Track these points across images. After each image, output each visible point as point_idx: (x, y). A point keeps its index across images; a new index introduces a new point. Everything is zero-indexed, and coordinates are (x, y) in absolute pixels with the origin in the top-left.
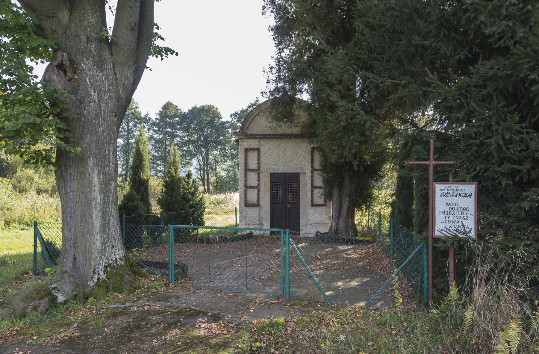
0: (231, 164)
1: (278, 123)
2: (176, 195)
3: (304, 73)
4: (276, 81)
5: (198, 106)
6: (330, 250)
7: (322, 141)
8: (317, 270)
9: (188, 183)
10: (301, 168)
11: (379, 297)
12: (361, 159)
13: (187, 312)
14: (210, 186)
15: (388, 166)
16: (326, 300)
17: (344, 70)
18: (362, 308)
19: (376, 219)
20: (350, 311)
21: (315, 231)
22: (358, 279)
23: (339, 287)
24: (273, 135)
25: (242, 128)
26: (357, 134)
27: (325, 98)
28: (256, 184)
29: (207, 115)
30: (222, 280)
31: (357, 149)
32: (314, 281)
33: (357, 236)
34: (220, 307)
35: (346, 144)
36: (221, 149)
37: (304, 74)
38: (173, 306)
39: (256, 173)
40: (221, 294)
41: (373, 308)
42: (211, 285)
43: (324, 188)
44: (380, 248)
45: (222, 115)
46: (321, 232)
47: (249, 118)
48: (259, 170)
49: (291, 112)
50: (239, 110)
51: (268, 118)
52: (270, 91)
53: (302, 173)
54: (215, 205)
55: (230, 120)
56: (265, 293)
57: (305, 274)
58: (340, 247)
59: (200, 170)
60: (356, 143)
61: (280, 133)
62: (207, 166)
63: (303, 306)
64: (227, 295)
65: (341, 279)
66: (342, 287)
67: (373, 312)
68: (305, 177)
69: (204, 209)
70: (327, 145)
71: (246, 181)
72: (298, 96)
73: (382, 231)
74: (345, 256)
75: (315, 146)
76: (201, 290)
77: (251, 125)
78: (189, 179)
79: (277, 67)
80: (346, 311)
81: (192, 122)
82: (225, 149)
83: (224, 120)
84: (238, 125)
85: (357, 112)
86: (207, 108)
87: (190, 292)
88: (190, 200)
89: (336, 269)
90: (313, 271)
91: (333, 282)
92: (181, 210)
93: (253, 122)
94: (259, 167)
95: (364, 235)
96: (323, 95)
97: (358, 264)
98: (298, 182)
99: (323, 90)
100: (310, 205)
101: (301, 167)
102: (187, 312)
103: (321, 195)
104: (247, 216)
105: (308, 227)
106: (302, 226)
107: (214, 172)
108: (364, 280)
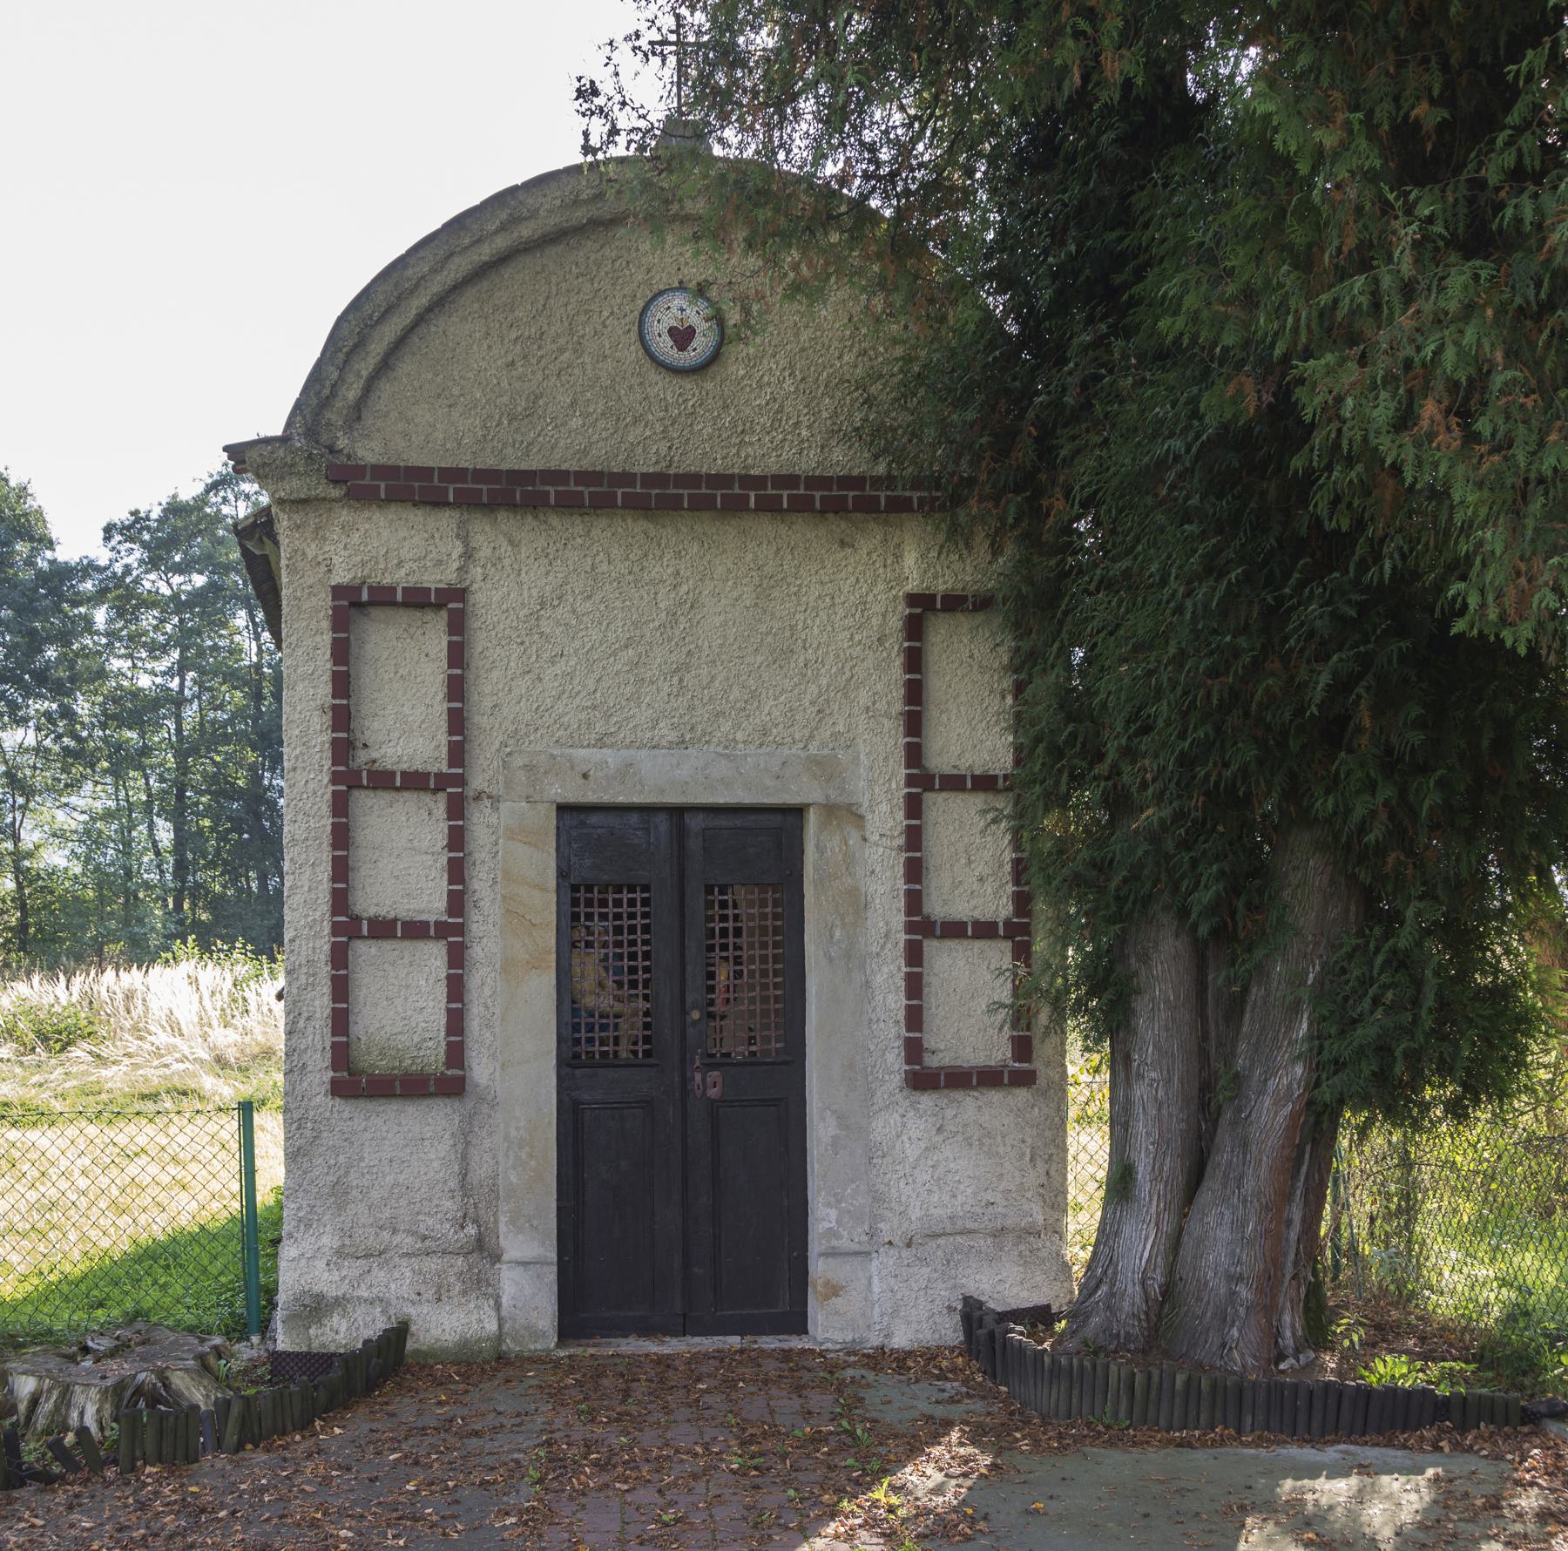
10: (824, 768)
21: (946, 1294)
28: (431, 902)
36: (47, 715)
39: (439, 805)
48: (461, 781)
55: (103, 556)
71: (341, 870)
77: (386, 389)
82: (67, 713)
83: (67, 552)
84: (148, 585)
93: (406, 367)
94: (457, 754)
100: (897, 1079)
104: (353, 1179)
105: (881, 1265)
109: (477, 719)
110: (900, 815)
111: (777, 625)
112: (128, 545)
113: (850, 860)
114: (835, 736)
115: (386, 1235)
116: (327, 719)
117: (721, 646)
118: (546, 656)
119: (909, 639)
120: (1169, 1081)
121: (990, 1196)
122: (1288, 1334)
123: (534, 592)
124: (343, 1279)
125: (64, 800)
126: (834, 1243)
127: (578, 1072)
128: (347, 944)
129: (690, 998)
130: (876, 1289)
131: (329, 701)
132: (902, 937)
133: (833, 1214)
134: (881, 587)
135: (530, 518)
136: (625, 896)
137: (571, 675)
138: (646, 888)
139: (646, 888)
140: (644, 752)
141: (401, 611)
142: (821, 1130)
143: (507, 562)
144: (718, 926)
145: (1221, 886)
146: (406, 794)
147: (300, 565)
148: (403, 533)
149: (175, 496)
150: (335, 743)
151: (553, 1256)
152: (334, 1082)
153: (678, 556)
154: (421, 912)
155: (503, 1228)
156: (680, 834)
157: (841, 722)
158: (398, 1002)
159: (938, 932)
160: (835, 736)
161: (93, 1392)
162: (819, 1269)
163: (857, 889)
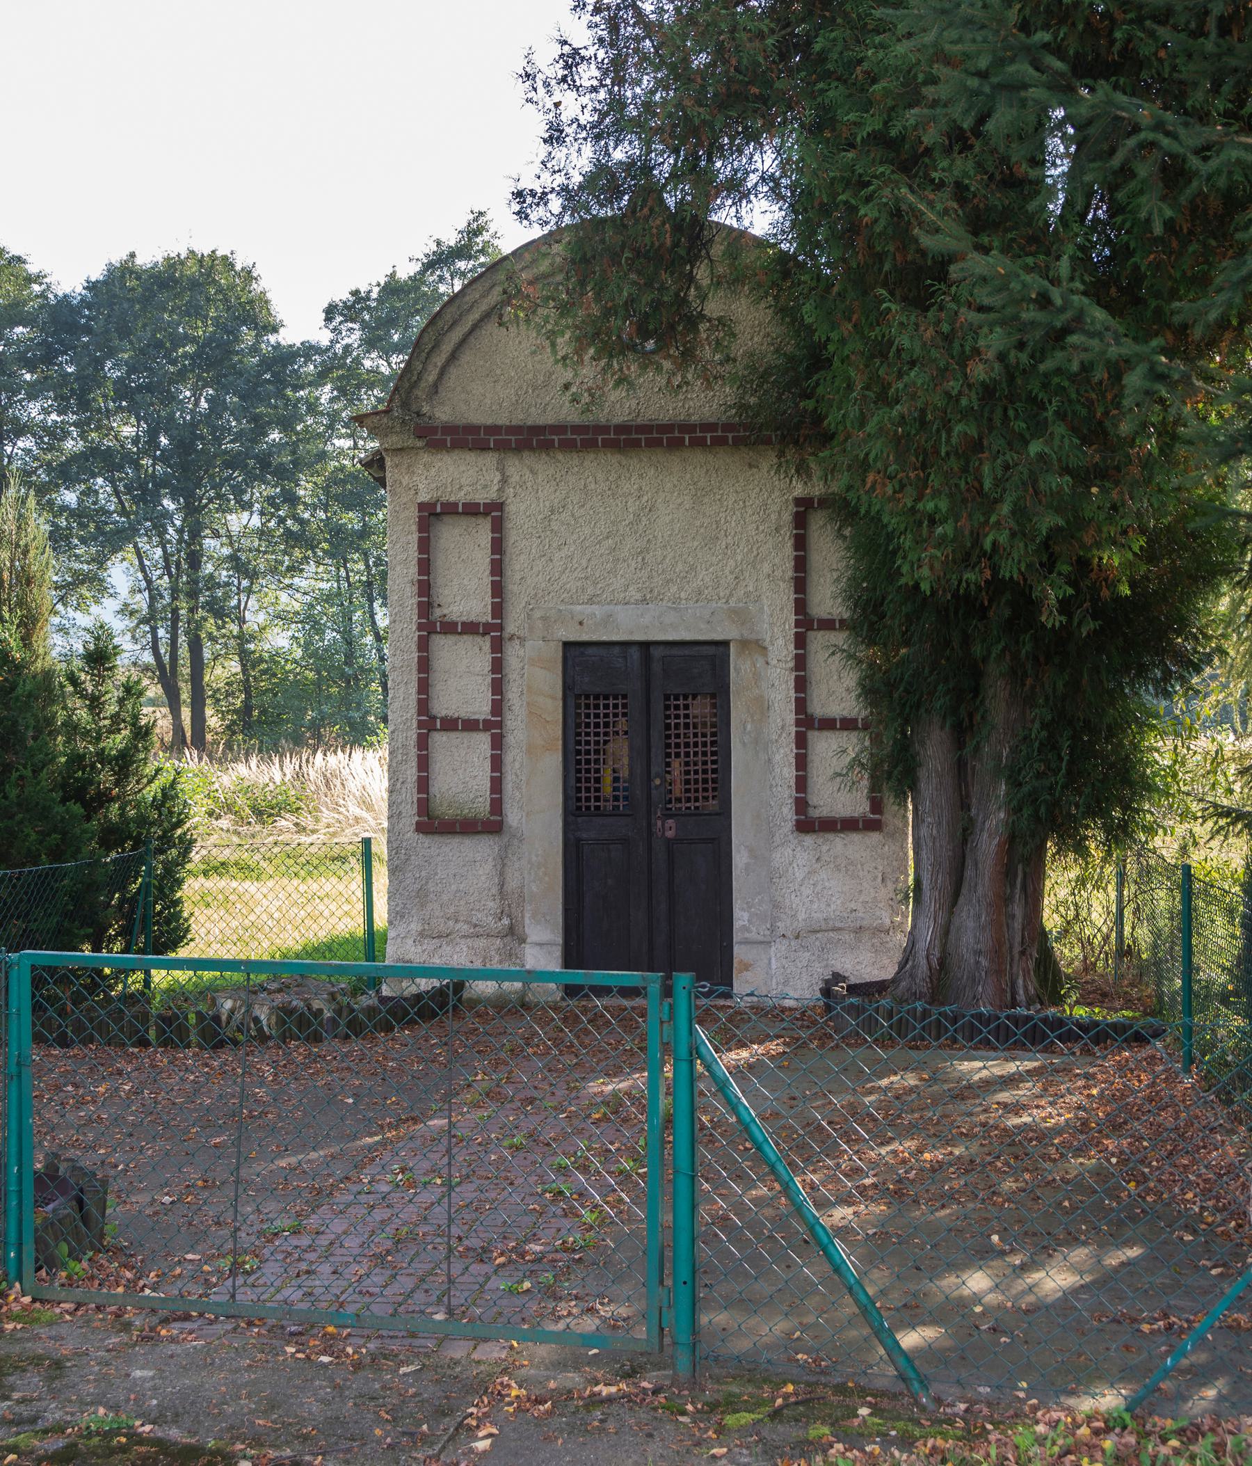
0: (325, 586)
1: (609, 365)
2: (28, 773)
3: (755, 90)
4: (597, 134)
5: (145, 259)
6: (911, 1080)
7: (864, 466)
8: (847, 1201)
9: (95, 703)
10: (739, 616)
11: (1202, 1357)
12: (1083, 565)
13: (112, 1452)
14: (209, 712)
15: (1224, 605)
16: (902, 1377)
17: (995, 80)
18: (1110, 1424)
19: (1163, 899)
20: (1040, 1440)
21: (821, 972)
22: (1080, 1254)
23: (977, 1298)
24: (577, 429)
25: (405, 384)
26: (1060, 429)
27: (878, 229)
28: (481, 708)
29: (194, 311)
30: (304, 1266)
31: (1058, 511)
32: (837, 1270)
33: (1058, 1000)
34: (302, 1422)
35: (997, 482)
36: (270, 500)
37: (758, 98)
38: (33, 1420)
39: (486, 643)
40: (301, 1347)
41: (1169, 1424)
42: (246, 1296)
43: (866, 727)
44: (1188, 1071)
45: (281, 308)
46: (853, 980)
47: (442, 335)
48: (501, 628)
49: (684, 301)
50: (370, 279)
51: (552, 336)
52: (565, 189)
53: (745, 644)
54: (241, 820)
55: (323, 337)
56: (556, 1337)
57: (780, 1222)
58: (966, 1066)
59: (150, 619)
60: (1058, 482)
61: (618, 420)
62: (193, 594)
63: (776, 1415)
64: (339, 1355)
65: (982, 1255)
66: (992, 1299)
67: (1174, 1443)
68: (760, 663)
69: (187, 845)
70: (889, 490)
71: (424, 686)
72: (724, 215)
73: (1198, 969)
74: (992, 1118)
75: (817, 489)
76: (188, 1325)
77: (453, 372)
78: (100, 680)
79: (601, 54)
80: (1018, 1440)
81: (111, 353)
82: (291, 499)
83: (289, 336)
84: (367, 364)
85: (1068, 315)
86: (192, 269)
87: (124, 1337)
88: (104, 798)
89: (952, 1197)
90: (822, 1204)
91: (935, 1274)
92: (57, 854)
93: (466, 357)
94: (498, 610)
95: (1096, 995)
96: (867, 212)
97: (1076, 1163)
98: (720, 694)
99: (868, 184)
100: (789, 825)
101: (735, 611)
102: (112, 1452)
103: (851, 767)
105: (778, 949)
106: (747, 942)
107: (235, 629)
108: (1114, 1258)
109: (510, 587)
110: (792, 647)
111: (707, 521)
112: (350, 325)
113: (757, 677)
114: (747, 594)
115: (451, 923)
116: (415, 589)
117: (670, 535)
118: (555, 545)
119: (796, 528)
120: (940, 824)
121: (853, 905)
122: (1021, 992)
123: (547, 504)
124: (424, 951)
125: (287, 581)
126: (747, 935)
127: (580, 820)
128: (428, 734)
129: (654, 770)
130: (774, 967)
131: (416, 577)
132: (793, 729)
133: (746, 915)
134: (777, 493)
135: (544, 456)
136: (611, 702)
137: (571, 557)
138: (625, 697)
139: (625, 697)
140: (619, 607)
141: (463, 518)
142: (740, 859)
143: (529, 484)
144: (673, 722)
145: (947, 698)
146: (465, 637)
147: (398, 490)
148: (462, 468)
149: (393, 275)
150: (420, 604)
151: (560, 940)
152: (418, 823)
153: (641, 476)
154: (475, 713)
155: (527, 921)
156: (647, 659)
157: (751, 584)
158: (460, 772)
159: (816, 725)
160: (747, 594)
161: (265, 1009)
162: (740, 952)
163: (762, 697)
